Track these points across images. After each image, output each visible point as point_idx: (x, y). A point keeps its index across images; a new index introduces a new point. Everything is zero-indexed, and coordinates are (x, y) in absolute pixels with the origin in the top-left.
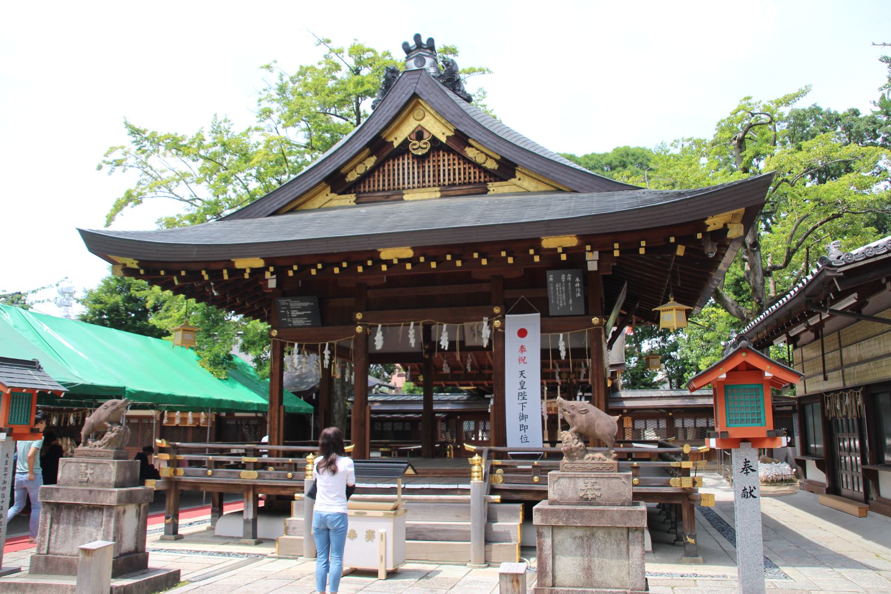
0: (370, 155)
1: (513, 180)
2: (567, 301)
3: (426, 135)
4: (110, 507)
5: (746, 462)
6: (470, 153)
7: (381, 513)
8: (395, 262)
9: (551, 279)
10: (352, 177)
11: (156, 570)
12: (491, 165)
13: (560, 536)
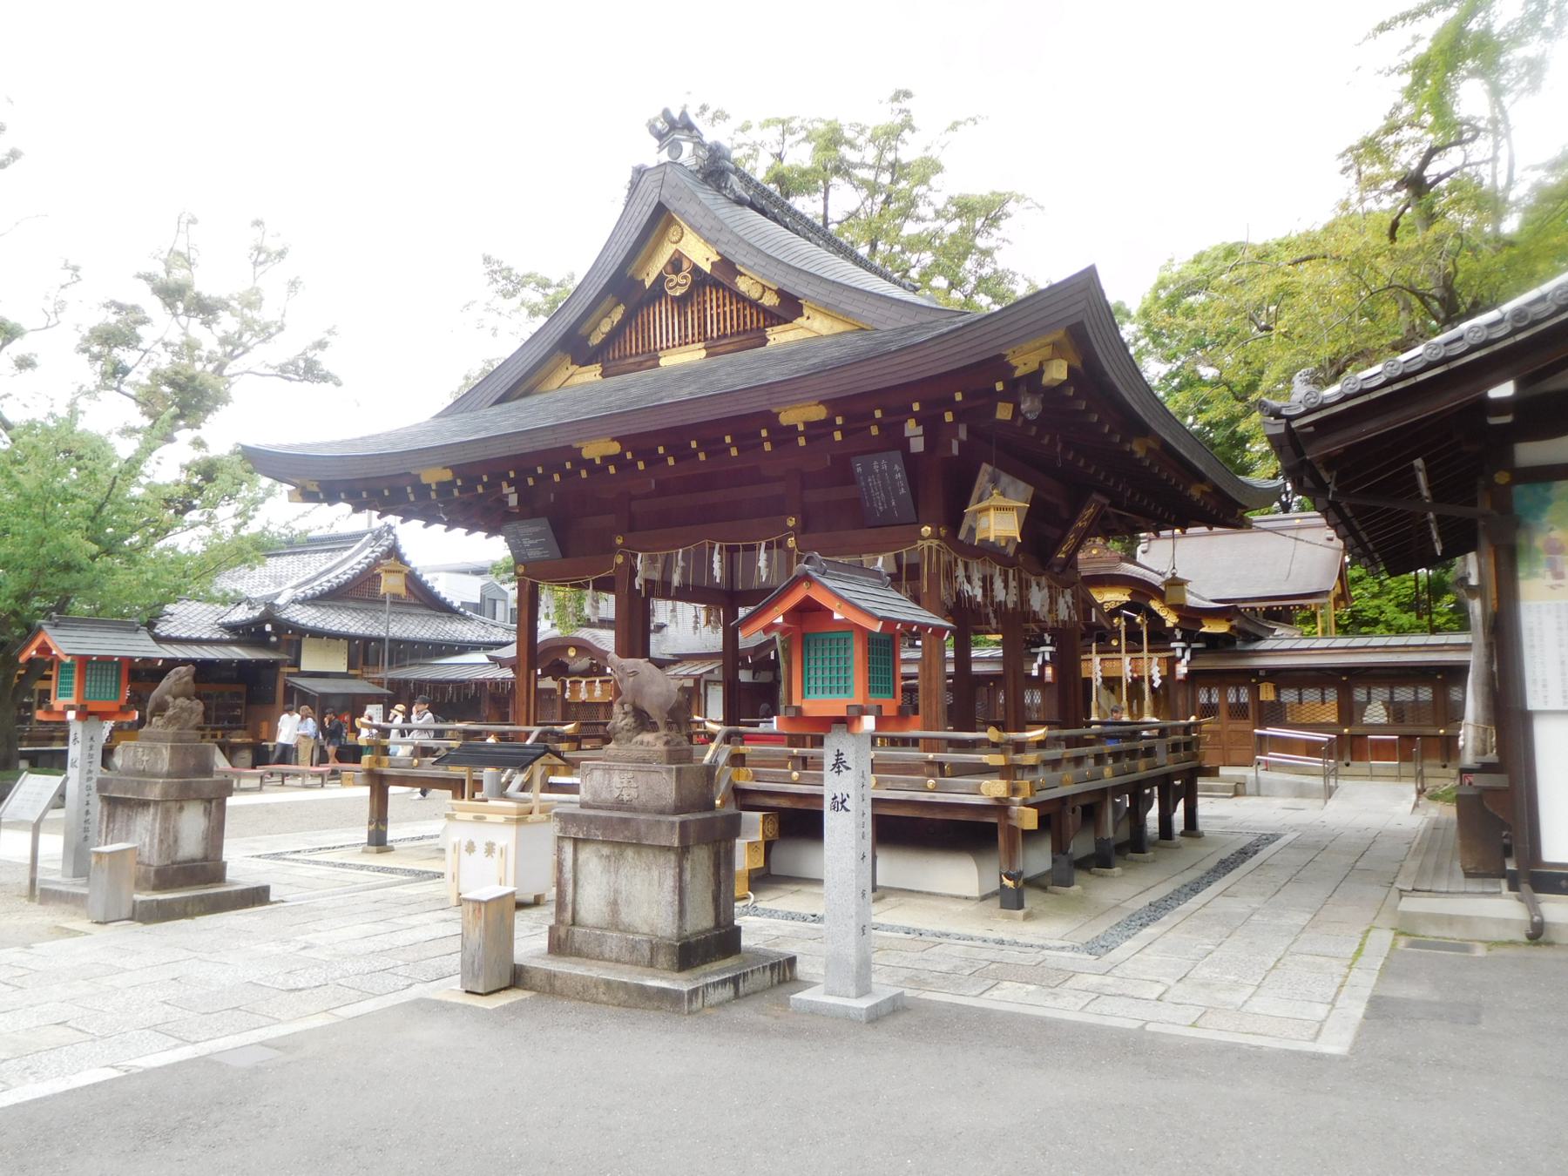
0: (618, 304)
1: (800, 320)
2: (889, 503)
3: (685, 265)
4: (156, 802)
5: (839, 754)
6: (743, 285)
7: (501, 818)
8: (598, 461)
9: (859, 470)
10: (596, 340)
11: (233, 883)
12: (770, 300)
13: (586, 853)
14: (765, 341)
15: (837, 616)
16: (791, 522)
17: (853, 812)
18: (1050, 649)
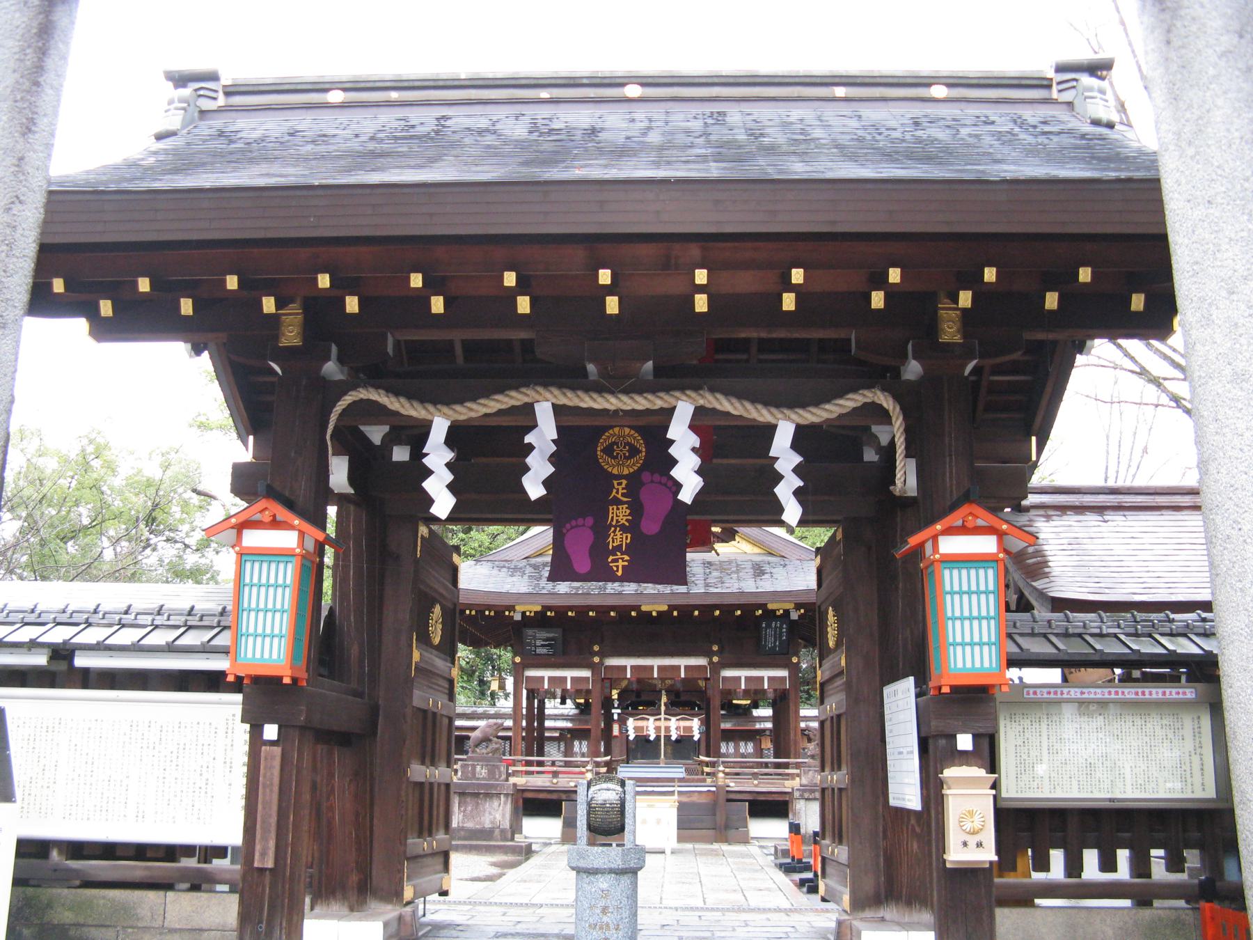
1: (733, 543)
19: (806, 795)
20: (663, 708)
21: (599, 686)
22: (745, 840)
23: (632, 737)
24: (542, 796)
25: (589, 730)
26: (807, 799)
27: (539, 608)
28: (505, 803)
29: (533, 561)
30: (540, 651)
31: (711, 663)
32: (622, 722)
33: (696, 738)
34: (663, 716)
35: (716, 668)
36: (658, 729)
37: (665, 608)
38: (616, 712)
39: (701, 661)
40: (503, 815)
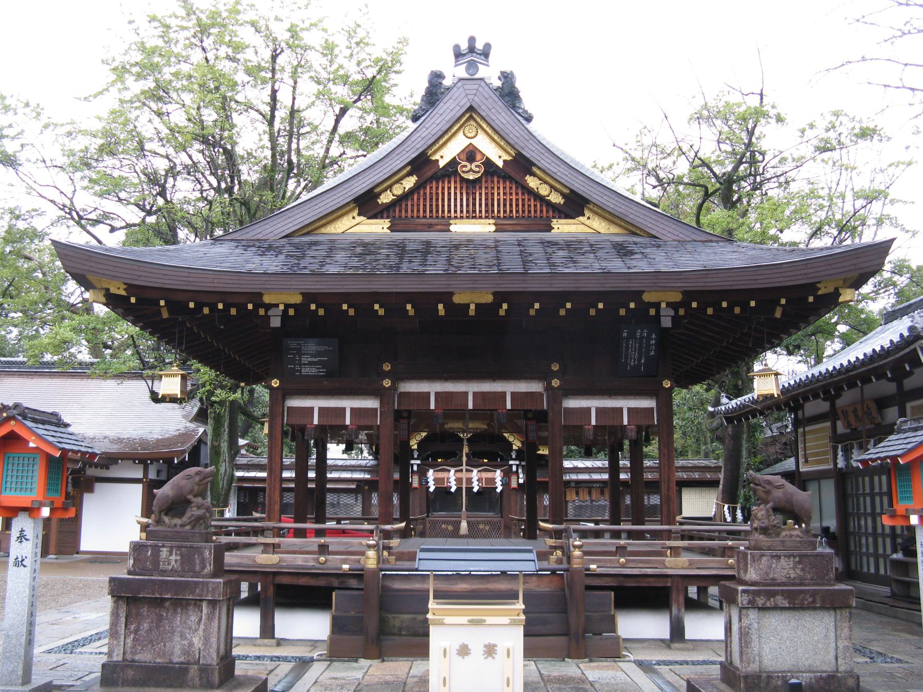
1: (581, 218)
2: (639, 360)
3: (478, 157)
9: (625, 335)
12: (556, 199)
14: (550, 229)
15: (32, 445)
16: (555, 367)
17: (28, 569)
18: (419, 462)
19: (760, 601)
20: (464, 459)
21: (391, 419)
22: (613, 651)
23: (432, 489)
24: (302, 581)
25: (547, 483)
26: (763, 609)
27: (297, 299)
28: (210, 619)
29: (296, 240)
30: (306, 371)
31: (549, 388)
32: (422, 473)
33: (499, 490)
34: (464, 467)
35: (556, 396)
36: (459, 481)
37: (489, 299)
38: (416, 462)
39: (535, 387)
40: (206, 639)
